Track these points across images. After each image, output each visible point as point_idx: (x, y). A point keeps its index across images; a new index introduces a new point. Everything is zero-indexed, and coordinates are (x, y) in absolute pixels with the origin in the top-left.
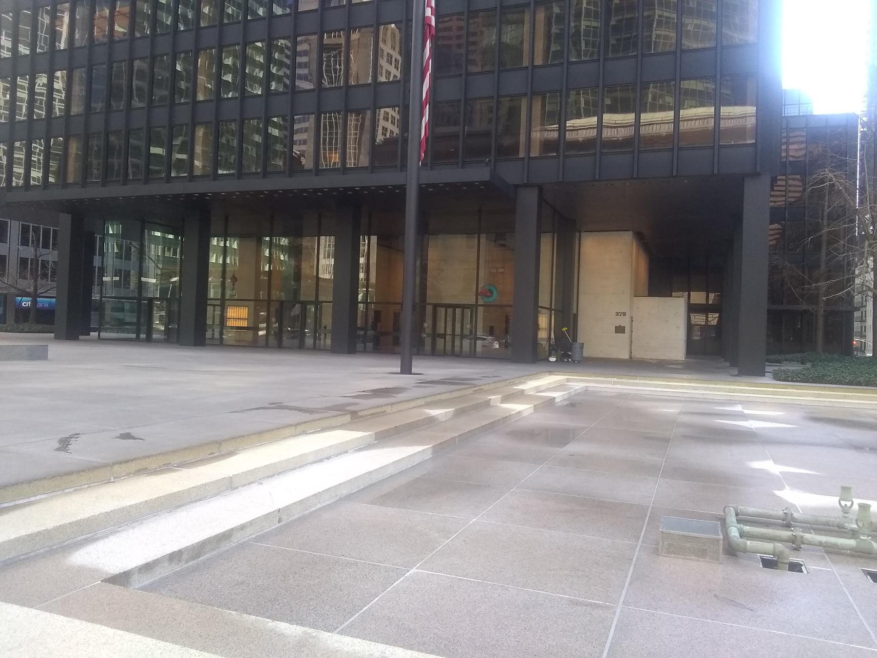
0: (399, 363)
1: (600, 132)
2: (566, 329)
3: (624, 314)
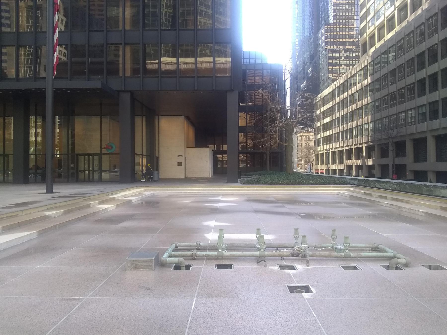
1: (160, 66)
2: (150, 164)
3: (182, 156)
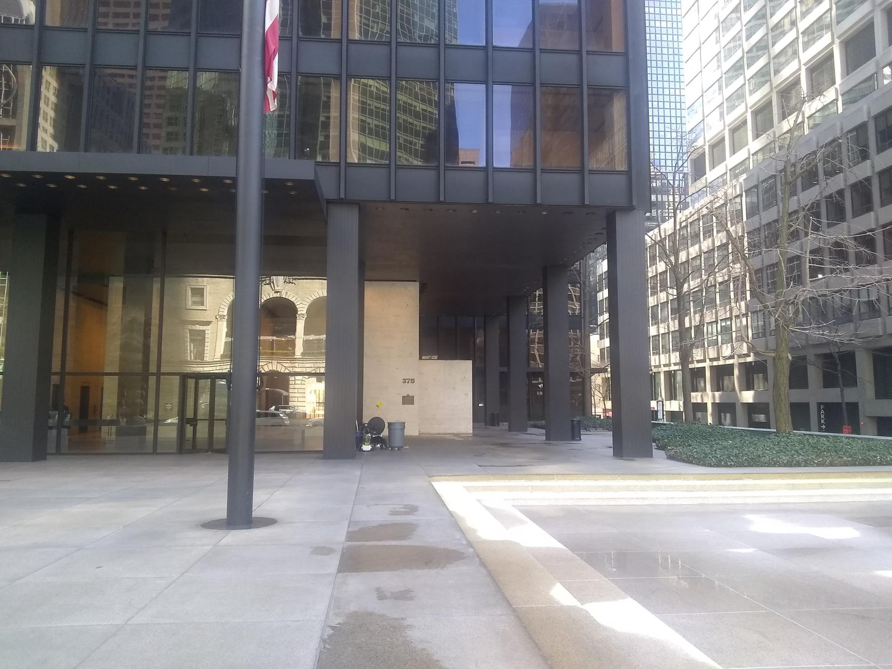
0: (227, 462)
